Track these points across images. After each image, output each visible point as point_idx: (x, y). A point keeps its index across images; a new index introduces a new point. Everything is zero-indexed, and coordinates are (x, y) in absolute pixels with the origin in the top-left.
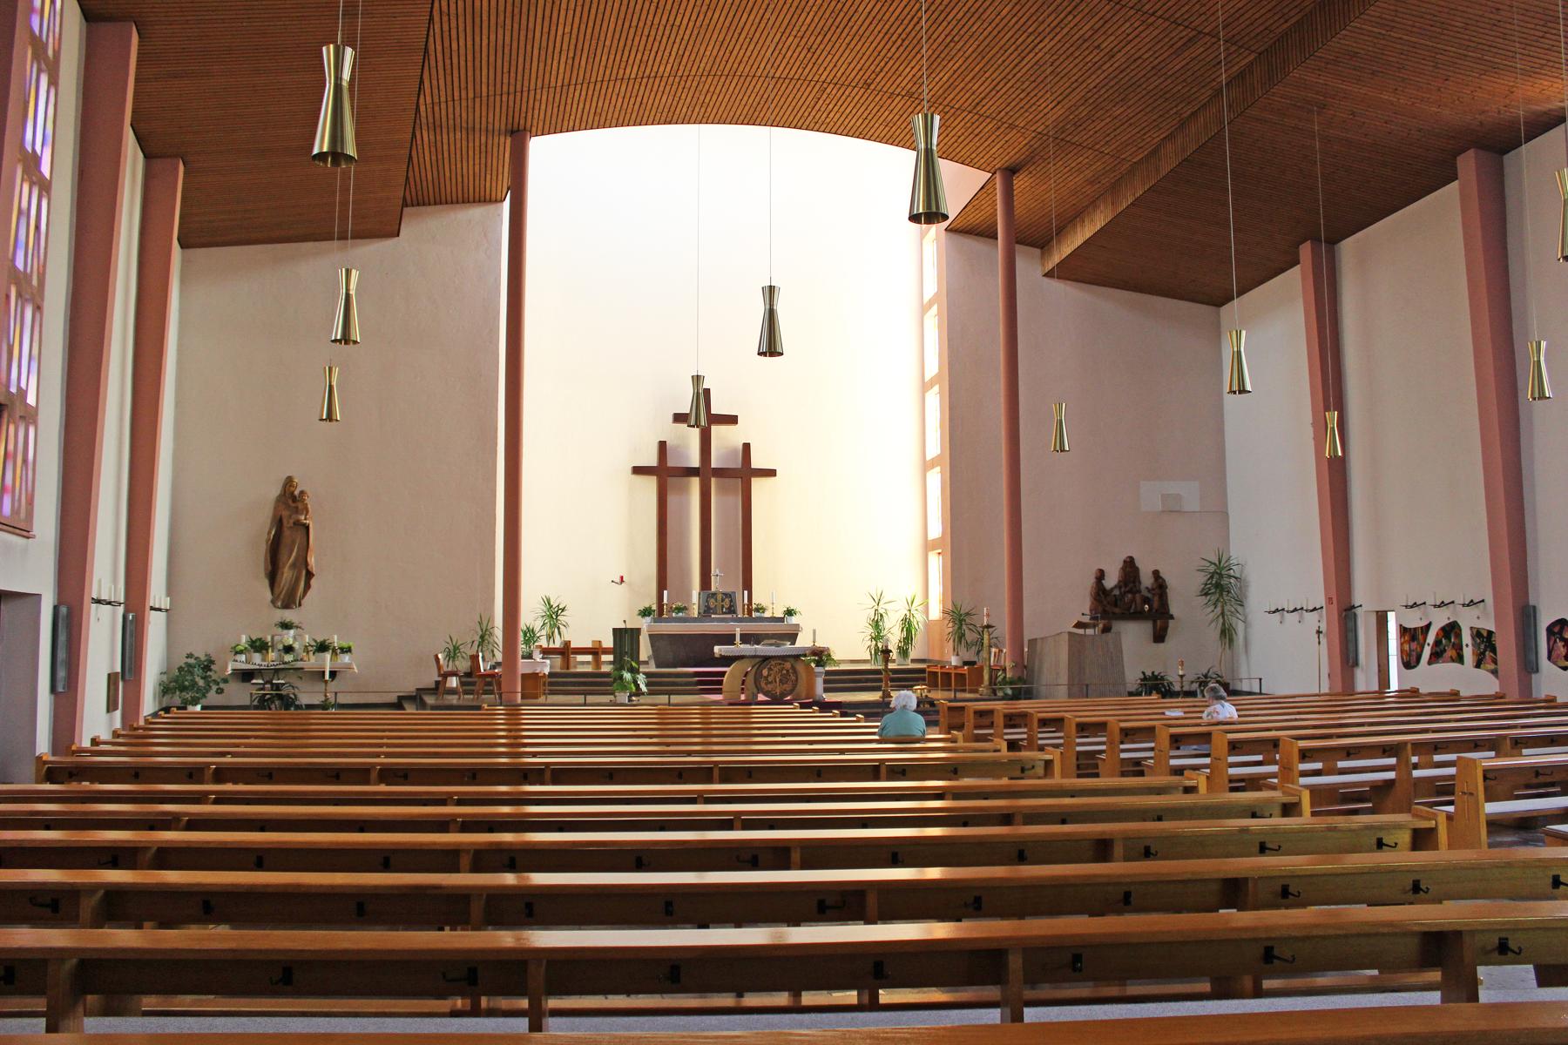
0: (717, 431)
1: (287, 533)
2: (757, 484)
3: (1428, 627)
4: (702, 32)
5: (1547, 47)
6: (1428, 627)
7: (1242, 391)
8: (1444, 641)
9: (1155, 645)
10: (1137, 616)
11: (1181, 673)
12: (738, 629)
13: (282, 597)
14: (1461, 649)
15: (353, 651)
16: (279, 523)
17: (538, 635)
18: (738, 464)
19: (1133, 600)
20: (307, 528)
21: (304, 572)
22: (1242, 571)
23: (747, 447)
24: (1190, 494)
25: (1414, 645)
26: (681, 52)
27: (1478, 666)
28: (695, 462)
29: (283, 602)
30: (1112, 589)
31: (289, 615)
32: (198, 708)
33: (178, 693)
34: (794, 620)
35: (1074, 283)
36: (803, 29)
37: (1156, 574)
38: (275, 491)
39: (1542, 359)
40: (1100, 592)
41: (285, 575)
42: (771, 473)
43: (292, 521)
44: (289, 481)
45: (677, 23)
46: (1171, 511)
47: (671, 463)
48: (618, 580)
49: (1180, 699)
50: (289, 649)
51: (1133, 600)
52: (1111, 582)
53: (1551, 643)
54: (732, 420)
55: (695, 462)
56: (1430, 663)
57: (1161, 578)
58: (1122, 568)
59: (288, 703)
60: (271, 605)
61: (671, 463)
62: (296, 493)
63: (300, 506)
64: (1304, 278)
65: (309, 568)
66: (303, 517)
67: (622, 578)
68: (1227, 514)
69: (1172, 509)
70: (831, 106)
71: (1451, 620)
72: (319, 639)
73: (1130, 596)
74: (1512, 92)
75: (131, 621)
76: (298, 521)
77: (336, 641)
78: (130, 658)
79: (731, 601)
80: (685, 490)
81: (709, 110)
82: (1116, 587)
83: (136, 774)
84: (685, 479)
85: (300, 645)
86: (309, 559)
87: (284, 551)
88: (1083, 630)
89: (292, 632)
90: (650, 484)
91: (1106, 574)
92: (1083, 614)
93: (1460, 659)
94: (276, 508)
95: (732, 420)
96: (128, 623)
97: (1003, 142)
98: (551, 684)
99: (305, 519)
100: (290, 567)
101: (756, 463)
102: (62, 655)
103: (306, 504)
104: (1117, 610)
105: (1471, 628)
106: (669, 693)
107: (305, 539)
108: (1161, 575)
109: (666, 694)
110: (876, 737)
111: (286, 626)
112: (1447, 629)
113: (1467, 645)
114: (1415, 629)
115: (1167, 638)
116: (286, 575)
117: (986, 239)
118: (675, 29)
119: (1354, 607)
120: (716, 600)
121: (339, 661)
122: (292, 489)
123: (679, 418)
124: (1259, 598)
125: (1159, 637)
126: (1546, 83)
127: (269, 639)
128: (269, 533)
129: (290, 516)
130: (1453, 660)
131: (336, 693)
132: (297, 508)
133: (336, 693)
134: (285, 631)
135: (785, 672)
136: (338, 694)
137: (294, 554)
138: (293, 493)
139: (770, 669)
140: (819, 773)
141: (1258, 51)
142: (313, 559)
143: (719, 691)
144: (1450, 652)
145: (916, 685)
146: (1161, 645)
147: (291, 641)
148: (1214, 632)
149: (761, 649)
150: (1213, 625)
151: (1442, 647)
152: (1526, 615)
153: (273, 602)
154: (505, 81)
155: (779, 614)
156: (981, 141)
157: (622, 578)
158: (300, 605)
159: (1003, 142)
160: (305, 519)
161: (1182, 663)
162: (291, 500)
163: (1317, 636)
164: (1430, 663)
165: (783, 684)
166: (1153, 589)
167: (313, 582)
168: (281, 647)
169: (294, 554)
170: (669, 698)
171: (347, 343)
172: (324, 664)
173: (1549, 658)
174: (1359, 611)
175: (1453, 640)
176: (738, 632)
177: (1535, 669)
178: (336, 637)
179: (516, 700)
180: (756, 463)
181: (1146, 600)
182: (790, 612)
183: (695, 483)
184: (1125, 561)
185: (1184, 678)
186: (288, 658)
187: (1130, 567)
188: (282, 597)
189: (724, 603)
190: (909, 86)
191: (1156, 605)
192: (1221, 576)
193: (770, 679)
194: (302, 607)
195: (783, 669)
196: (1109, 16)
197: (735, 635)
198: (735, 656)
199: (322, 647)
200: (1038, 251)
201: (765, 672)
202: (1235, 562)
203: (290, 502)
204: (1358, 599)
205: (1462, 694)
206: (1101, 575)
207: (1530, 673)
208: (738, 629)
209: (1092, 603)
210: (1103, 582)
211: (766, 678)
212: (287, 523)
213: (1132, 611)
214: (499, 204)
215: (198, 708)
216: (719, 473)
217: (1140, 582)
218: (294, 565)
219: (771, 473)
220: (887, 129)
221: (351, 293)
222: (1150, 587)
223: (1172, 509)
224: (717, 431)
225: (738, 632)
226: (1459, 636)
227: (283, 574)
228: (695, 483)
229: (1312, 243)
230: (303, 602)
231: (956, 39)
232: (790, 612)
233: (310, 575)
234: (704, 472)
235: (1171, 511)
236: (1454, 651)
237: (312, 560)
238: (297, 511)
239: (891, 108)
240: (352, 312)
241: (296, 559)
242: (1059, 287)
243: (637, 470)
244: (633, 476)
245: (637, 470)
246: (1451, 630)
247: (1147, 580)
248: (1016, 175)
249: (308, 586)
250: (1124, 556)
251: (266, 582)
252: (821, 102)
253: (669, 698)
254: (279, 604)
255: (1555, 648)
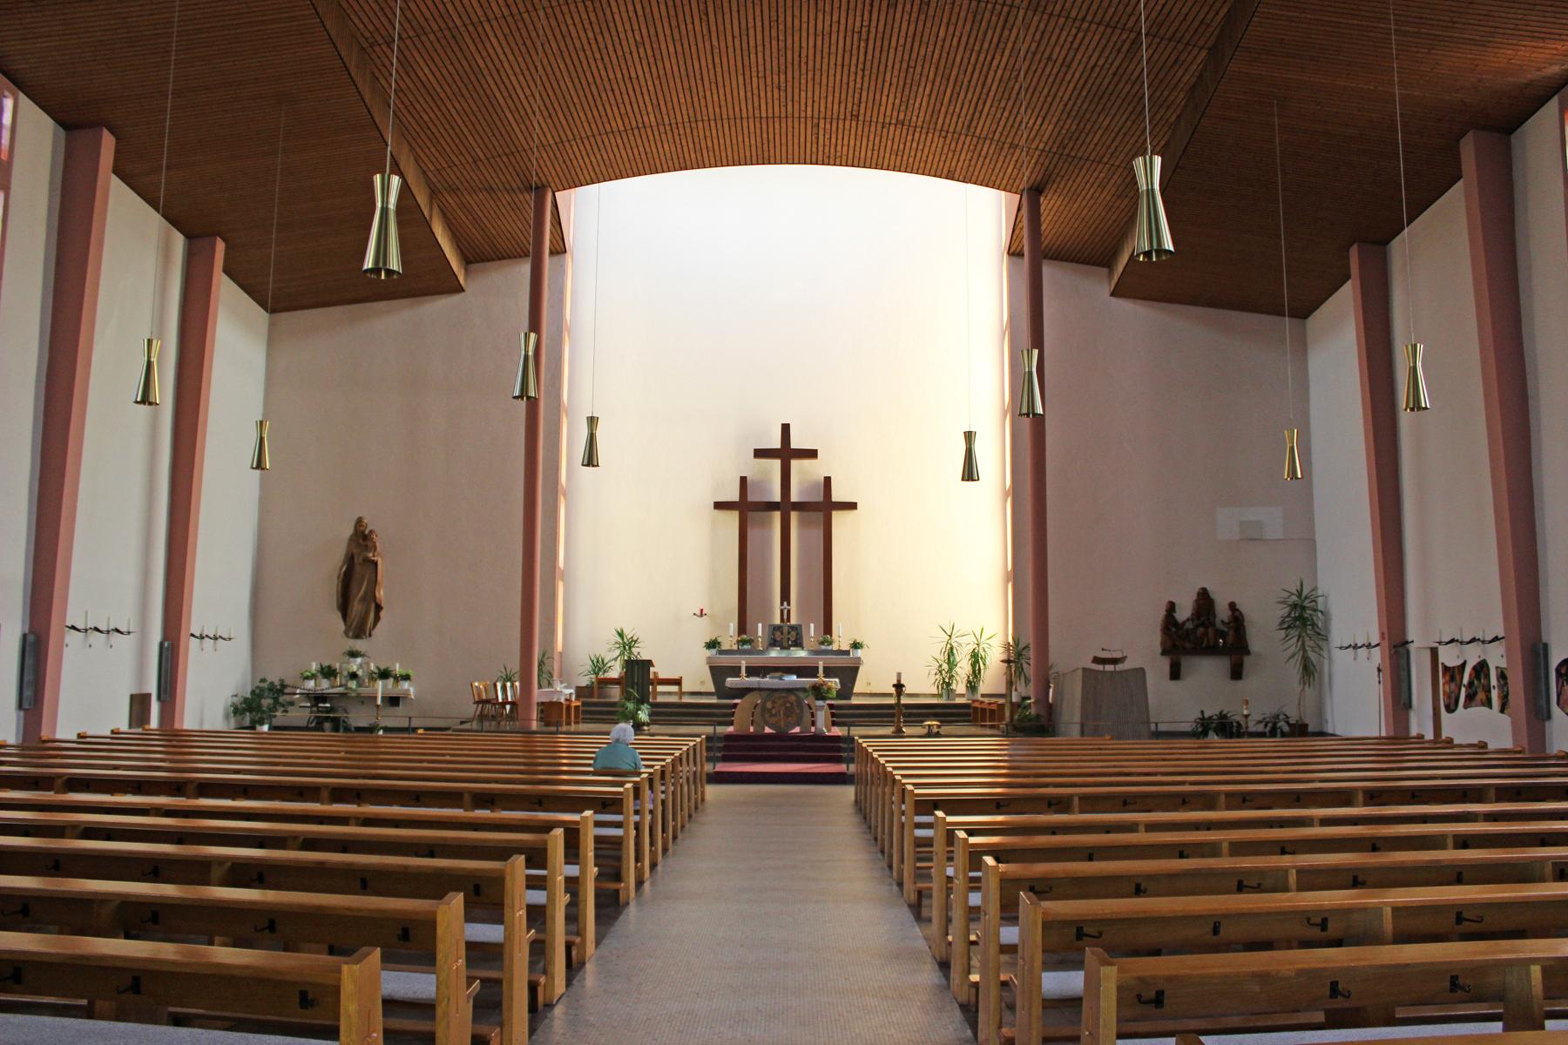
0: (795, 464)
1: (358, 569)
2: (837, 517)
3: (1464, 664)
4: (664, 81)
5: (1485, 13)
6: (1464, 664)
7: (1420, 408)
8: (1476, 682)
9: (1234, 682)
10: (1211, 650)
11: (1245, 712)
12: (743, 662)
13: (353, 626)
14: (1489, 691)
15: (412, 678)
16: (350, 560)
17: (608, 665)
18: (819, 498)
19: (1206, 634)
20: (376, 564)
21: (373, 606)
22: (1326, 603)
23: (828, 480)
24: (1271, 520)
25: (1453, 686)
26: (655, 102)
27: (1502, 711)
28: (777, 498)
29: (354, 633)
30: (1184, 623)
31: (359, 645)
32: (266, 728)
33: (248, 714)
34: (859, 653)
35: (1143, 302)
36: (761, 68)
37: (1232, 606)
38: (348, 531)
39: (1419, 364)
40: (1170, 622)
41: (355, 609)
42: (852, 506)
43: (361, 558)
44: (359, 522)
45: (634, 75)
46: (1251, 539)
47: (751, 498)
48: (698, 613)
49: (1245, 740)
50: (353, 676)
51: (1206, 634)
52: (1184, 613)
53: (1560, 686)
54: (812, 454)
55: (777, 498)
56: (1465, 707)
57: (1238, 610)
58: (1196, 601)
59: (337, 724)
60: (343, 635)
61: (751, 498)
62: (367, 532)
63: (369, 543)
64: (1354, 288)
65: (378, 601)
66: (371, 555)
67: (702, 610)
68: (1315, 541)
69: (1252, 537)
70: (833, 140)
71: (1482, 659)
72: (382, 667)
73: (1201, 629)
74: (1477, 66)
75: (167, 649)
76: (367, 557)
77: (398, 669)
78: (166, 682)
79: (797, 634)
80: (767, 525)
81: (717, 153)
82: (1188, 620)
83: (176, 788)
84: (769, 513)
85: (363, 672)
86: (377, 593)
87: (354, 586)
88: (1113, 666)
89: (359, 660)
90: (733, 518)
91: (1177, 607)
92: (1103, 649)
93: (1488, 703)
94: (349, 545)
95: (812, 454)
96: (164, 650)
97: (1013, 163)
98: (613, 713)
99: (374, 556)
100: (360, 600)
101: (837, 496)
102: (1404, 685)
103: (375, 542)
104: (1188, 645)
105: (1497, 668)
106: (849, 725)
107: (374, 575)
108: (1238, 607)
109: (712, 725)
110: (591, 769)
111: (353, 654)
112: (1478, 668)
113: (1494, 687)
114: (1453, 668)
115: (1244, 673)
116: (356, 607)
117: (1050, 261)
118: (635, 82)
119: (1407, 643)
120: (782, 633)
121: (399, 687)
122: (362, 528)
123: (760, 453)
124: (1340, 633)
125: (1236, 673)
126: (1509, 52)
127: (337, 666)
128: (341, 569)
129: (360, 554)
130: (1483, 704)
131: (410, 718)
132: (367, 546)
133: (410, 718)
134: (352, 659)
135: (788, 705)
136: (412, 719)
137: (363, 588)
138: (363, 532)
139: (774, 702)
140: (417, 797)
141: (1207, 46)
142: (382, 592)
143: (731, 723)
144: (1481, 696)
145: (926, 721)
146: (1240, 683)
147: (354, 668)
148: (1294, 670)
149: (768, 681)
150: (1293, 661)
151: (1474, 689)
152: (1535, 652)
153: (346, 633)
154: (496, 144)
155: (845, 647)
156: (993, 163)
157: (702, 610)
158: (370, 635)
159: (1013, 163)
160: (374, 556)
161: (1247, 702)
162: (362, 538)
163: (1377, 673)
164: (1465, 707)
165: (788, 717)
166: (1228, 624)
167: (382, 614)
168: (345, 673)
169: (363, 588)
170: (849, 732)
171: (144, 404)
172: (377, 690)
173: (1558, 704)
174: (1412, 647)
175: (1482, 681)
176: (743, 664)
177: (1545, 715)
178: (398, 665)
179: (530, 725)
180: (837, 496)
181: (1223, 635)
182: (856, 645)
183: (777, 515)
184: (1198, 594)
185: (1249, 718)
186: (353, 684)
187: (1204, 600)
188: (353, 626)
189: (790, 636)
190: (895, 114)
191: (1230, 639)
192: (1304, 608)
193: (774, 711)
194: (373, 637)
195: (785, 703)
196: (1042, 26)
197: (740, 667)
198: (747, 688)
199: (384, 674)
200: (1105, 270)
201: (769, 705)
202: (1320, 593)
203: (361, 541)
204: (1412, 634)
205: (1456, 742)
206: (1171, 607)
207: (1544, 721)
208: (743, 662)
209: (1162, 638)
210: (1175, 614)
211: (770, 711)
212: (358, 560)
213: (1204, 646)
214: (561, 256)
215: (266, 728)
216: (799, 506)
217: (1215, 616)
218: (364, 599)
219: (852, 506)
220: (899, 158)
221: (152, 360)
222: (1226, 620)
223: (1252, 537)
224: (795, 464)
225: (743, 664)
226: (1487, 676)
227: (353, 606)
228: (777, 515)
229: (1359, 247)
230: (373, 633)
231: (912, 64)
232: (856, 645)
233: (379, 608)
234: (785, 506)
235: (1251, 539)
236: (1483, 694)
237: (381, 593)
238: (366, 548)
239: (891, 137)
240: (152, 372)
241: (366, 592)
242: (1125, 306)
243: (719, 506)
244: (716, 511)
245: (719, 506)
246: (1481, 668)
247: (1223, 613)
248: (1044, 194)
249: (377, 618)
250: (1196, 589)
251: (339, 615)
252: (821, 137)
253: (849, 732)
254: (351, 634)
255: (1563, 692)
